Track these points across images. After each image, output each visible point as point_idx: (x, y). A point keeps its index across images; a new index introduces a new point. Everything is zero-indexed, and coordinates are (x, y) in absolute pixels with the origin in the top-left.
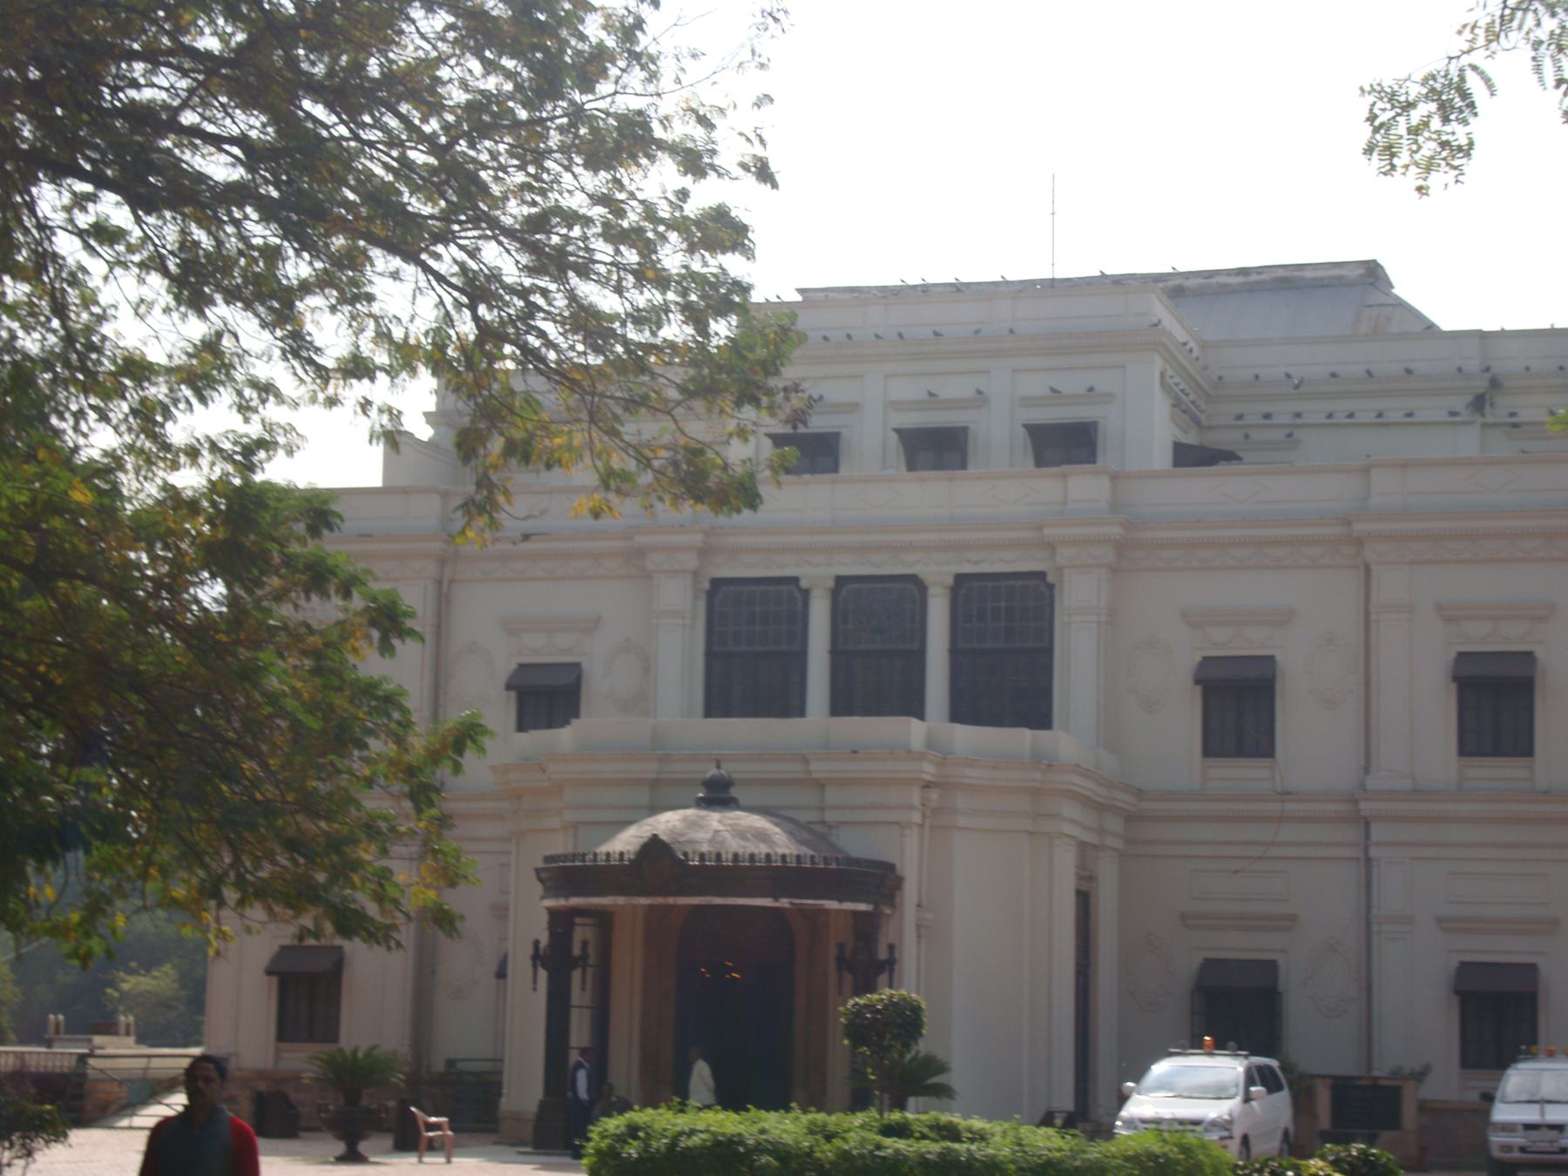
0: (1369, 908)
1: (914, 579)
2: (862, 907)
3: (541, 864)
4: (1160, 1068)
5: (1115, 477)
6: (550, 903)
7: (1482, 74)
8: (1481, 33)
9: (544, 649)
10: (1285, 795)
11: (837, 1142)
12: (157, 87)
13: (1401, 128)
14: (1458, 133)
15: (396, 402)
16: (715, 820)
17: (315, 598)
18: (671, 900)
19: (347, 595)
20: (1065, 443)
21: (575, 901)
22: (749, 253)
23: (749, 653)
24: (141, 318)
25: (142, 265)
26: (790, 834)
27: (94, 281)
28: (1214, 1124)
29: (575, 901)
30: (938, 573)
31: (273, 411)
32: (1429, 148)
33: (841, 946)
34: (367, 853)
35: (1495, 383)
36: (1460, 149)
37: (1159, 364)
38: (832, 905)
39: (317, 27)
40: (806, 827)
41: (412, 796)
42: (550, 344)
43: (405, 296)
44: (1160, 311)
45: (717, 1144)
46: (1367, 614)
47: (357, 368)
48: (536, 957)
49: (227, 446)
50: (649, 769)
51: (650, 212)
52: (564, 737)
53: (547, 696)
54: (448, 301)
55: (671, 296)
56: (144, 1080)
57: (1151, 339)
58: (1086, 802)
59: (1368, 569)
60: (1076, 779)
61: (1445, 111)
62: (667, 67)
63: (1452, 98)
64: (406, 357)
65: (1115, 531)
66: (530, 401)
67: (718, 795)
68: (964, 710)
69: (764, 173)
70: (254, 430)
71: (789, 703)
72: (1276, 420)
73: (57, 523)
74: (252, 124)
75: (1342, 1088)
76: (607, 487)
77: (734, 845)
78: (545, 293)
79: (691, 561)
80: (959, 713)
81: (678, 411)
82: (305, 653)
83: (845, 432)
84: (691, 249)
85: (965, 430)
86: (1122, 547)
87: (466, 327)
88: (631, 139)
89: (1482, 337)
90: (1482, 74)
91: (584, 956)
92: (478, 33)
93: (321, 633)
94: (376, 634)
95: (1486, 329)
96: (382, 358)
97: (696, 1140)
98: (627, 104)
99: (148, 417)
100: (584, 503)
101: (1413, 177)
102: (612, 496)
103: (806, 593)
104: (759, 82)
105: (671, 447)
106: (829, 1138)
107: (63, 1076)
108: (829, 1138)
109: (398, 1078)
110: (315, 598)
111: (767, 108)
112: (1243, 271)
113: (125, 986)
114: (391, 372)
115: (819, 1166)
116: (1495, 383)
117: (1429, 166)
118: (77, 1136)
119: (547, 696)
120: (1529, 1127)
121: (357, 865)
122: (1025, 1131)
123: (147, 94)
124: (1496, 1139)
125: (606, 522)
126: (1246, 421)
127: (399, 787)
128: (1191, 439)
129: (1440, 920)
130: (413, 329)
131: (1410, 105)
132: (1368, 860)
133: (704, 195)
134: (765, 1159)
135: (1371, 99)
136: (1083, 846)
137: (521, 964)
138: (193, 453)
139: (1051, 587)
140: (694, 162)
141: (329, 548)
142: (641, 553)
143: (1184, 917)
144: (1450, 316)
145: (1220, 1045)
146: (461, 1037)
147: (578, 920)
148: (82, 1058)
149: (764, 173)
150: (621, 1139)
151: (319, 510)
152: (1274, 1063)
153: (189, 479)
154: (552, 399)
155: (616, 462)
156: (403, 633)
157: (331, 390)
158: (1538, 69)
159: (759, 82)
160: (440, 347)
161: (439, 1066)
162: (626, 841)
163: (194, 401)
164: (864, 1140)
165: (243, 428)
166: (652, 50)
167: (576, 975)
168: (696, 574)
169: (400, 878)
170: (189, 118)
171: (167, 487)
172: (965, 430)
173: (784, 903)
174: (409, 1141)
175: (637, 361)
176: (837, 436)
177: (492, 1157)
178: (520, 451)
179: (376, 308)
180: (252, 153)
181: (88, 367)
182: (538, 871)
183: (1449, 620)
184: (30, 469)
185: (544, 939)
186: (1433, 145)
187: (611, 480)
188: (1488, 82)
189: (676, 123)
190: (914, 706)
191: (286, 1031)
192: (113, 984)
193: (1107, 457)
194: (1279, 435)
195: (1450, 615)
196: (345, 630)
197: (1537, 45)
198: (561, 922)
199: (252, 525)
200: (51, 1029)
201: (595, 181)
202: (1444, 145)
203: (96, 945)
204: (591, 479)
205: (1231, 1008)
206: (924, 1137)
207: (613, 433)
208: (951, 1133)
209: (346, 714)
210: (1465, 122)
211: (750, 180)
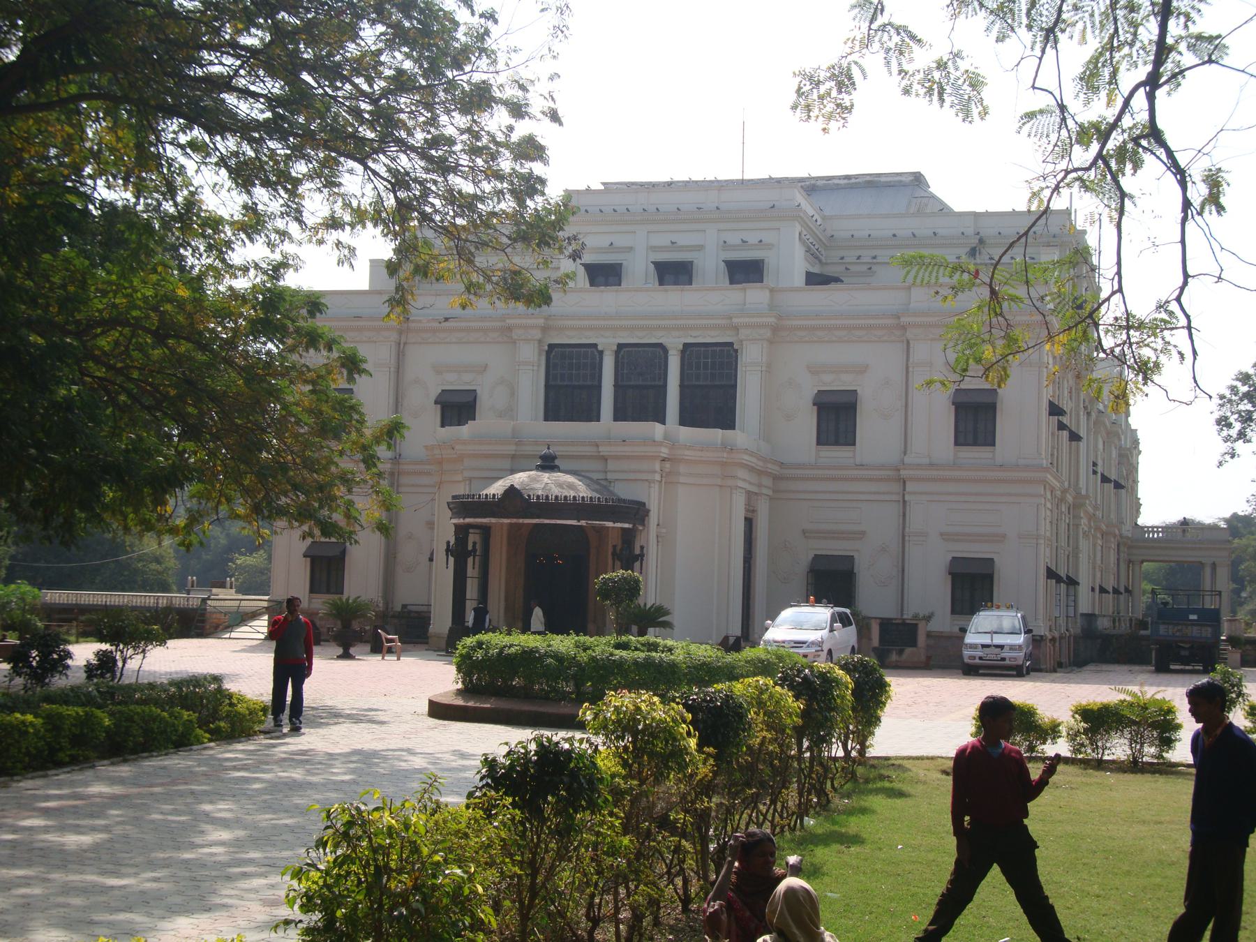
0: (904, 528)
1: (660, 345)
2: (626, 526)
3: (450, 500)
4: (787, 614)
5: (772, 291)
6: (455, 521)
7: (860, 66)
8: (857, 43)
9: (456, 382)
10: (861, 466)
11: (590, 652)
12: (220, 65)
13: (815, 96)
14: (846, 99)
15: (353, 243)
16: (546, 477)
17: (312, 351)
18: (521, 521)
19: (330, 349)
20: (745, 271)
21: (468, 520)
22: (546, 162)
23: (569, 385)
24: (219, 196)
25: (217, 164)
26: (588, 485)
27: (190, 171)
28: (813, 643)
29: (468, 520)
30: (674, 344)
31: (288, 247)
32: (830, 107)
33: (614, 547)
34: (340, 491)
35: (981, 241)
36: (846, 108)
37: (798, 228)
38: (610, 524)
39: (310, 32)
40: (597, 482)
41: (364, 461)
42: (436, 211)
43: (356, 182)
44: (800, 198)
45: (524, 652)
46: (907, 368)
47: (333, 223)
48: (448, 550)
49: (264, 266)
50: (510, 449)
51: (493, 139)
52: (465, 430)
53: (457, 408)
54: (381, 188)
55: (505, 185)
56: (237, 612)
57: (795, 214)
58: (752, 469)
59: (908, 342)
60: (746, 457)
61: (840, 86)
62: (502, 58)
63: (843, 79)
64: (360, 217)
65: (772, 320)
66: (426, 242)
67: (548, 463)
68: (687, 419)
69: (554, 117)
70: (277, 257)
71: (590, 413)
72: (863, 260)
73: (168, 307)
74: (274, 87)
75: (885, 624)
76: (469, 292)
77: (556, 491)
78: (435, 182)
79: (537, 334)
80: (683, 422)
81: (509, 250)
82: (306, 382)
83: (625, 263)
84: (515, 159)
85: (691, 263)
86: (775, 329)
87: (390, 202)
88: (480, 98)
89: (976, 215)
90: (860, 66)
91: (474, 549)
92: (398, 37)
93: (314, 370)
94: (345, 373)
95: (978, 210)
96: (347, 218)
97: (513, 650)
98: (477, 77)
99: (220, 248)
100: (457, 301)
101: (821, 123)
102: (471, 297)
103: (601, 353)
104: (550, 66)
105: (504, 271)
106: (585, 650)
107: (193, 609)
108: (585, 650)
109: (371, 614)
110: (312, 351)
111: (556, 81)
112: (848, 177)
113: (238, 562)
114: (353, 226)
115: (579, 664)
116: (981, 241)
117: (830, 117)
118: (170, 643)
119: (457, 408)
120: (984, 646)
121: (334, 498)
122: (693, 647)
123: (216, 69)
124: (966, 653)
125: (469, 311)
126: (847, 260)
127: (359, 456)
128: (816, 270)
129: (941, 534)
130: (362, 201)
131: (818, 83)
132: (904, 502)
133: (523, 129)
134: (549, 660)
135: (799, 79)
136: (749, 493)
137: (440, 555)
138: (245, 270)
139: (736, 351)
140: (518, 110)
141: (319, 324)
142: (510, 329)
143: (804, 532)
144: (959, 203)
145: (818, 601)
146: (408, 594)
148: (204, 600)
149: (554, 117)
150: (473, 649)
151: (314, 303)
152: (848, 611)
153: (241, 284)
154: (440, 244)
155: (475, 277)
156: (361, 372)
157: (319, 236)
158: (888, 63)
159: (550, 66)
160: (378, 212)
161: (398, 608)
162: (497, 488)
163: (247, 241)
164: (603, 651)
165: (272, 256)
166: (494, 47)
167: (470, 560)
168: (540, 341)
169: (359, 506)
170: (242, 82)
171: (231, 288)
172: (691, 263)
173: (583, 523)
174: (378, 648)
175: (486, 221)
176: (621, 265)
177: (1053, 681)
178: (422, 271)
179: (342, 190)
180: (272, 102)
181: (191, 218)
182: (448, 504)
184: (154, 277)
185: (452, 542)
186: (832, 105)
187: (471, 288)
188: (863, 71)
189: (507, 88)
190: (659, 416)
191: (315, 587)
192: (232, 560)
193: (769, 279)
194: (865, 268)
196: (329, 370)
197: (888, 50)
198: (462, 531)
199: (276, 309)
200: (189, 584)
201: (461, 120)
202: (838, 105)
203: (194, 539)
204: (462, 288)
205: (831, 582)
206: (636, 649)
207: (470, 262)
208: (653, 647)
209: (337, 417)
210: (849, 93)
211: (547, 120)
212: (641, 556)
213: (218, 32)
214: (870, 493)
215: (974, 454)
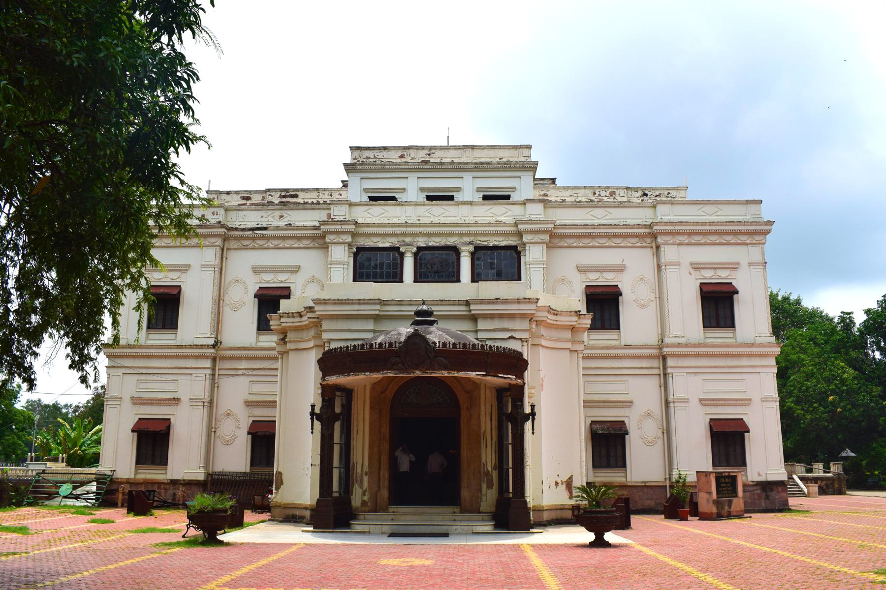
48: (312, 414)
129: (700, 400)
147: (338, 393)
183: (696, 269)
195: (697, 267)
198: (328, 393)
212: (533, 414)
214: (642, 368)
215: (719, 336)
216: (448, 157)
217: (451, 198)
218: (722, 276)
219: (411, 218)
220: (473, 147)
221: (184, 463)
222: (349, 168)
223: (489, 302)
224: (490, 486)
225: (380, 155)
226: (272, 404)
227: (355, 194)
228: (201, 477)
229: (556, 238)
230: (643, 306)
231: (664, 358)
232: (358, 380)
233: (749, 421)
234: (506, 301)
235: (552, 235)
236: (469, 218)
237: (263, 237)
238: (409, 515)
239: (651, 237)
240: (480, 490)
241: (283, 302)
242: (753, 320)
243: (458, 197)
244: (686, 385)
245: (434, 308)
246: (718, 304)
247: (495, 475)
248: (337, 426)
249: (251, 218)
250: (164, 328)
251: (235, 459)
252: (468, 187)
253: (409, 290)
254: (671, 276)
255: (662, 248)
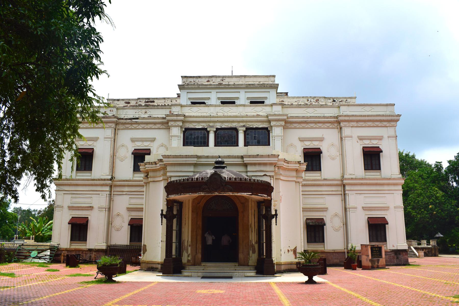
48: (162, 215)
129: (363, 208)
147: (175, 204)
183: (360, 139)
195: (361, 138)
198: (170, 204)
212: (276, 215)
213: (24, 89)
214: (332, 191)
215: (372, 174)
216: (232, 81)
217: (234, 103)
218: (374, 143)
219: (213, 113)
220: (245, 76)
221: (95, 240)
222: (181, 87)
223: (254, 156)
224: (254, 252)
225: (197, 80)
226: (141, 210)
227: (184, 100)
228: (104, 248)
229: (288, 124)
230: (333, 159)
231: (344, 186)
232: (185, 197)
233: (388, 219)
234: (262, 156)
235: (286, 122)
236: (243, 113)
237: (136, 123)
238: (212, 267)
239: (337, 123)
240: (249, 254)
241: (147, 157)
242: (390, 166)
243: (237, 102)
244: (356, 200)
245: (225, 160)
246: (372, 158)
247: (256, 246)
248: (175, 221)
249: (130, 113)
250: (85, 170)
251: (122, 238)
252: (243, 97)
253: (212, 150)
254: (348, 143)
255: (343, 129)
